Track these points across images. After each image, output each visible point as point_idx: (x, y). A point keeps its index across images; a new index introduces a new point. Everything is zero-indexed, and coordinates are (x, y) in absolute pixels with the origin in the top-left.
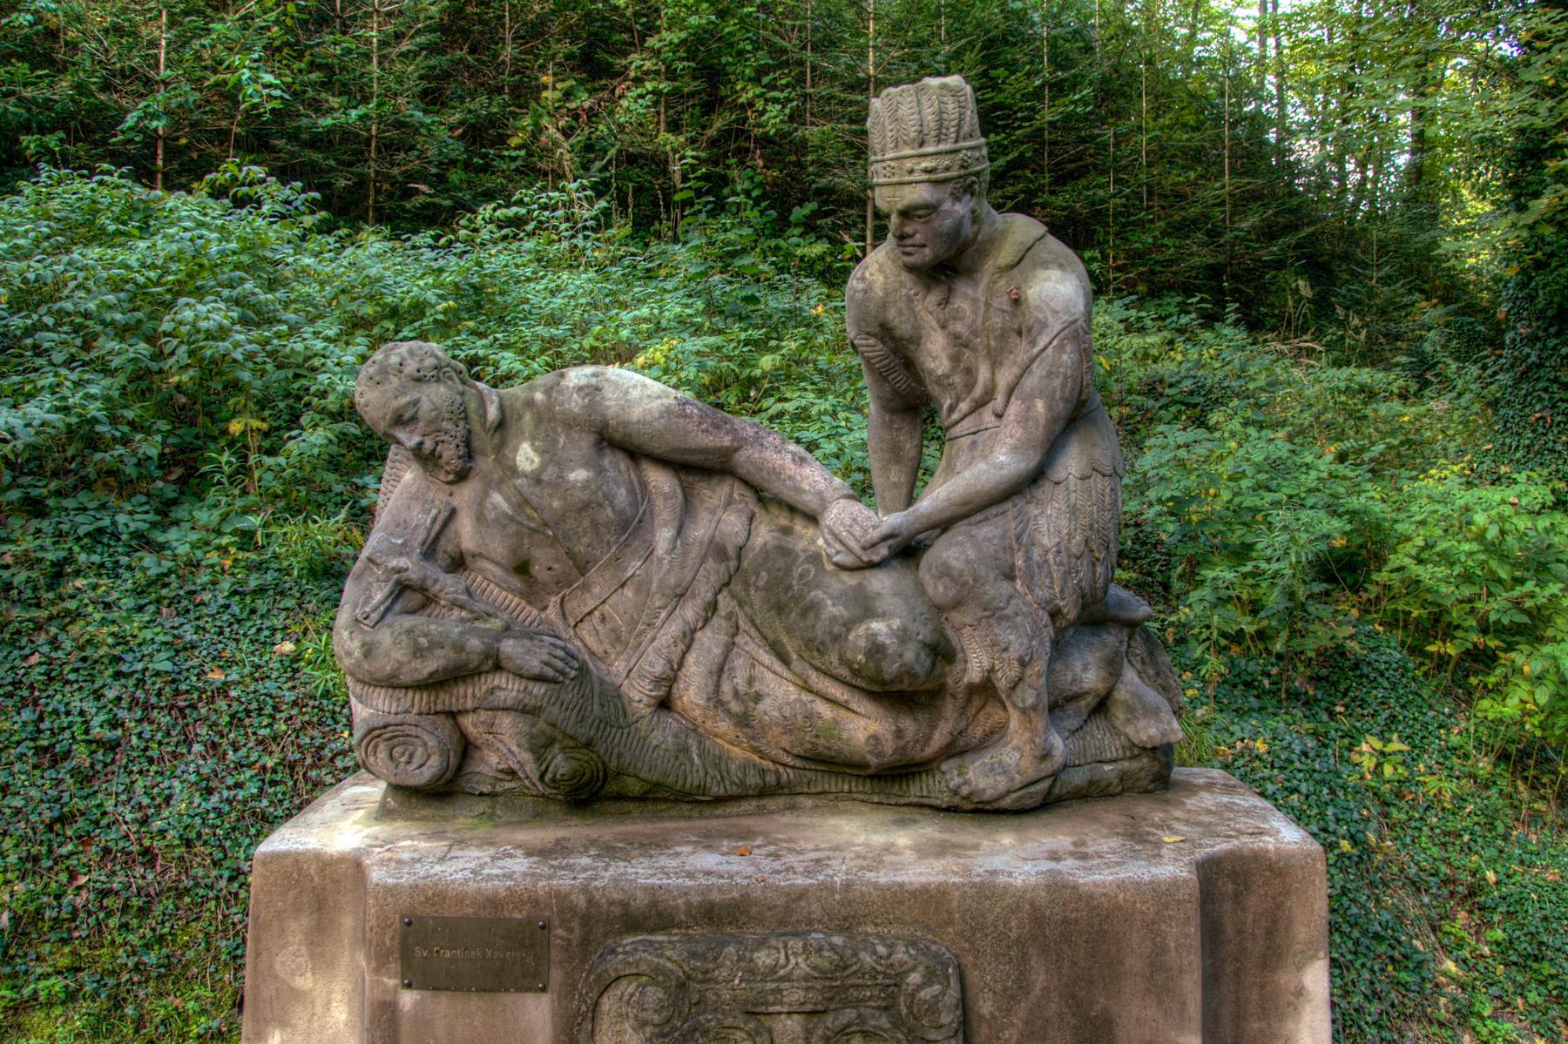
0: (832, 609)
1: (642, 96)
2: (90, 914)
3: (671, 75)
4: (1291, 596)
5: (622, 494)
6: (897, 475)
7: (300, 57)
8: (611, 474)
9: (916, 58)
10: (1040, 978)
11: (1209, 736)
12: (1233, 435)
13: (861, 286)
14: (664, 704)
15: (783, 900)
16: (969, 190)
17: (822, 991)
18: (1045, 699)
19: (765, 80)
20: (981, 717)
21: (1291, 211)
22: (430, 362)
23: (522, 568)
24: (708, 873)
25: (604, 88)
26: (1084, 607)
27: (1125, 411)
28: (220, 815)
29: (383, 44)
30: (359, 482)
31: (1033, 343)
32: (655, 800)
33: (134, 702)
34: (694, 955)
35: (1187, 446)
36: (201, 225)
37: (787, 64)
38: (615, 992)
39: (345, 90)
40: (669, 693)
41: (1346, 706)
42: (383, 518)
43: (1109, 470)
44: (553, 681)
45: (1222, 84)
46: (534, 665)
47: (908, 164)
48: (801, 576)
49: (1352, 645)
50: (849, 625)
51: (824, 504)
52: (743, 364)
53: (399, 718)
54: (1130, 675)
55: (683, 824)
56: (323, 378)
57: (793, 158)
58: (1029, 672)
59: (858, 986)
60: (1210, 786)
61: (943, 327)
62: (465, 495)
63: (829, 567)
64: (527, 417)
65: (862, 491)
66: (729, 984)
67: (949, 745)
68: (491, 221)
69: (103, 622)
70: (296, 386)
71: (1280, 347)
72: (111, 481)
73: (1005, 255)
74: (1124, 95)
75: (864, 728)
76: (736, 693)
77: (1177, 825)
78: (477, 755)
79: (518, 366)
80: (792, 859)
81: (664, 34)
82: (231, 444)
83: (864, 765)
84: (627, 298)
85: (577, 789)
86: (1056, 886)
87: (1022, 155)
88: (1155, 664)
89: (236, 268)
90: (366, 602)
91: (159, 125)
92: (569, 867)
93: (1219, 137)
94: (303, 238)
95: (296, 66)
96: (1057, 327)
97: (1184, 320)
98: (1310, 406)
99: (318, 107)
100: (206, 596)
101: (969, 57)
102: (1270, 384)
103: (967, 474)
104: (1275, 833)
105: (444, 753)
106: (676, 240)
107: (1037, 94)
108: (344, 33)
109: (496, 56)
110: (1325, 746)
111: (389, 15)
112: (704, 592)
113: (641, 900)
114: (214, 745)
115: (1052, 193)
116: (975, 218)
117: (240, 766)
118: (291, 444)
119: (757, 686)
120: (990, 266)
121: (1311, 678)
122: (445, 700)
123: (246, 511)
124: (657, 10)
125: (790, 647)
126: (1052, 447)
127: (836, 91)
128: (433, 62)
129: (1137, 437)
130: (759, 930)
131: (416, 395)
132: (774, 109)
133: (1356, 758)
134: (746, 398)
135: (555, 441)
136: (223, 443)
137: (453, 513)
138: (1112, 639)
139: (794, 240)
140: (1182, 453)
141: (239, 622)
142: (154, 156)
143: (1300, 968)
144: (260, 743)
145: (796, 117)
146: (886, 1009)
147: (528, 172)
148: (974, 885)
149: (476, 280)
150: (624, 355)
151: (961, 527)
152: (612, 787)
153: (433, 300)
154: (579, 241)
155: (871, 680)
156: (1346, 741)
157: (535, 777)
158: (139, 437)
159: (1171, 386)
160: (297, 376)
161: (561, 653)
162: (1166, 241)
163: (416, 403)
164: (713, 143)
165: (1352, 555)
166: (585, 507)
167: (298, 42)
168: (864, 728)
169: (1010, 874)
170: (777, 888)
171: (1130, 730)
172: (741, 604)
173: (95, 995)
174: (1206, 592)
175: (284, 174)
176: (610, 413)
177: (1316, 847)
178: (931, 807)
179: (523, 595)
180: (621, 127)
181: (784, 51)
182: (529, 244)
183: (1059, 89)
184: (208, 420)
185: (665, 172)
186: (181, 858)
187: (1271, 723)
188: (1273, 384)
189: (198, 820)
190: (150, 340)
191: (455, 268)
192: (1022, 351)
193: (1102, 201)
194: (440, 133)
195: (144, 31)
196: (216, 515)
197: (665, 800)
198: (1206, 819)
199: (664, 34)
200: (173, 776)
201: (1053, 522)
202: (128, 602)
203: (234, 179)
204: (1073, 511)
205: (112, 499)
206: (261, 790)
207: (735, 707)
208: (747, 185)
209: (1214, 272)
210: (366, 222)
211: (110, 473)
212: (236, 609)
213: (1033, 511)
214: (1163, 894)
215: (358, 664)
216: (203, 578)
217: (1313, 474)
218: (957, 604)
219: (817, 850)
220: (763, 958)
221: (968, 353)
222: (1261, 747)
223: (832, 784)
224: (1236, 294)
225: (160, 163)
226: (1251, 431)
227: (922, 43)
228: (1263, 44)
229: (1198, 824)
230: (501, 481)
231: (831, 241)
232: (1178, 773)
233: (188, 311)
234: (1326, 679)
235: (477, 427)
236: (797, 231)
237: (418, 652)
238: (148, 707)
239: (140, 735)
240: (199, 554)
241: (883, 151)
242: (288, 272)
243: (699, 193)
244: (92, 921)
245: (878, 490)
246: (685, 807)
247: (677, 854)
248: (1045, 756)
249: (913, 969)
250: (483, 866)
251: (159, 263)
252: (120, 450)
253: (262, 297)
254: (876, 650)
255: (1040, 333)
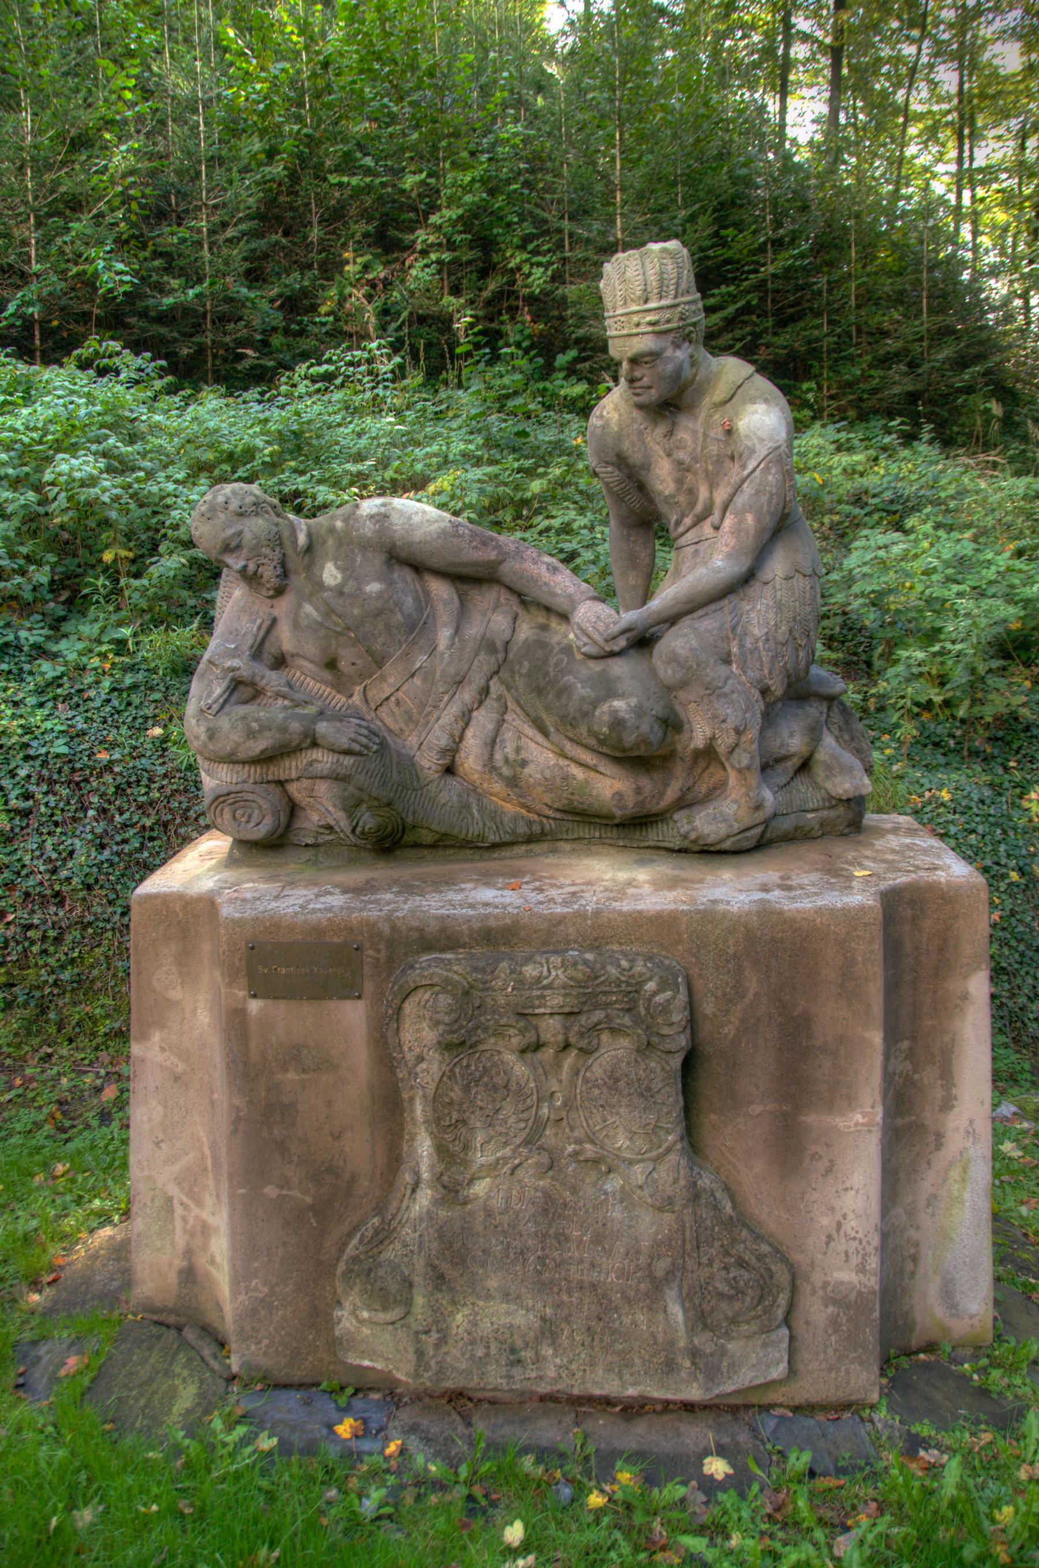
0: (582, 691)
1: (427, 266)
2: (18, 943)
3: (451, 246)
4: (973, 671)
5: (409, 602)
6: (634, 578)
7: (144, 247)
8: (400, 585)
9: (656, 222)
10: (752, 984)
11: (902, 787)
12: (926, 536)
13: (599, 423)
14: (450, 770)
15: (545, 926)
16: (687, 338)
17: (577, 997)
18: (757, 760)
19: (530, 247)
20: (705, 775)
21: (981, 343)
22: (249, 499)
23: (331, 665)
24: (486, 905)
25: (396, 260)
26: (789, 685)
27: (836, 518)
28: (112, 865)
29: (212, 232)
30: (208, 596)
31: (744, 467)
32: (445, 847)
33: (41, 779)
34: (475, 969)
35: (886, 547)
36: (72, 392)
37: (547, 232)
38: (414, 999)
39: (182, 273)
40: (453, 761)
41: (1019, 762)
42: (219, 628)
43: (809, 571)
44: (359, 754)
45: (921, 233)
46: (344, 742)
47: (635, 319)
48: (556, 664)
49: (1024, 712)
50: (595, 704)
51: (574, 605)
52: (517, 488)
53: (239, 788)
54: (829, 741)
55: (467, 866)
56: (175, 514)
57: (556, 313)
58: (743, 739)
59: (605, 993)
60: (895, 830)
61: (669, 455)
62: (283, 607)
63: (579, 657)
64: (330, 542)
65: (607, 595)
66: (503, 990)
67: (680, 799)
68: (306, 377)
69: (14, 717)
70: (154, 521)
71: (967, 461)
72: (14, 604)
73: (719, 393)
74: (836, 246)
75: (609, 787)
76: (507, 760)
77: (867, 863)
78: (302, 814)
79: (331, 497)
80: (553, 893)
81: (444, 211)
82: (106, 570)
83: (611, 817)
84: (420, 437)
85: (381, 840)
86: (765, 912)
87: (748, 302)
88: (850, 731)
89: (102, 427)
90: (209, 696)
91: (34, 311)
92: (376, 902)
93: (919, 281)
94: (155, 399)
95: (142, 255)
96: (764, 452)
97: (887, 440)
98: (993, 510)
99: (161, 289)
100: (92, 693)
101: (702, 220)
102: (959, 493)
103: (690, 577)
104: (945, 868)
105: (276, 814)
106: (460, 385)
107: (762, 249)
108: (179, 225)
109: (305, 238)
110: (1000, 795)
111: (216, 207)
112: (478, 679)
113: (433, 927)
114: (105, 811)
115: (775, 334)
116: (693, 362)
117: (125, 826)
118: (152, 569)
119: (523, 755)
120: (707, 402)
121: (990, 739)
122: (276, 772)
123: (120, 624)
124: (438, 191)
125: (549, 721)
126: (761, 553)
127: (590, 254)
128: (254, 245)
129: (846, 540)
130: (527, 949)
131: (239, 527)
132: (538, 272)
133: (1026, 804)
134: (519, 516)
135: (354, 561)
136: (99, 569)
137: (274, 621)
138: (814, 710)
139: (558, 383)
140: (882, 553)
141: (119, 712)
142: (33, 336)
143: (965, 977)
144: (140, 807)
145: (557, 278)
146: (629, 1010)
147: (337, 335)
148: (698, 912)
149: (295, 427)
150: (415, 484)
151: (686, 621)
152: (409, 838)
153: (261, 444)
154: (380, 391)
155: (614, 748)
156: (1018, 791)
157: (348, 830)
158: (32, 568)
159: (874, 496)
160: (155, 513)
161: (365, 732)
162: (872, 372)
163: (240, 533)
164: (489, 303)
165: (1026, 636)
166: (379, 613)
167: (142, 235)
168: (609, 787)
169: (728, 903)
170: (541, 916)
171: (828, 785)
172: (509, 688)
173: (26, 1005)
174: (900, 668)
175: (137, 346)
176: (397, 536)
177: (980, 880)
178: (671, 850)
179: (334, 686)
180: (412, 293)
181: (545, 221)
182: (338, 396)
183: (778, 244)
184: (87, 552)
185: (449, 329)
186: (84, 899)
187: (954, 776)
188: (961, 494)
189: (95, 870)
190: (38, 488)
191: (278, 417)
192: (735, 473)
193: (817, 340)
194: (262, 305)
195: (16, 233)
196: (96, 628)
197: (453, 847)
198: (890, 857)
199: (444, 211)
200: (74, 836)
201: (761, 615)
202: (31, 701)
203: (97, 353)
204: (779, 606)
205: (15, 619)
206: (142, 844)
207: (506, 771)
208: (518, 338)
209: (913, 397)
210: (206, 383)
211: (12, 597)
212: (115, 703)
213: (746, 606)
214: (851, 917)
215: (205, 746)
216: (89, 679)
217: (993, 568)
218: (684, 684)
219: (573, 884)
220: (530, 971)
221: (690, 477)
222: (945, 796)
223: (585, 832)
224: (929, 417)
225: (38, 342)
226: (941, 533)
227: (661, 210)
228: (959, 196)
229: (884, 861)
230: (311, 594)
231: (590, 382)
232: (870, 818)
233: (65, 465)
234: (1001, 739)
235: (290, 551)
236: (561, 375)
237: (251, 734)
238: (51, 782)
239: (47, 804)
240: (85, 659)
241: (614, 309)
242: (143, 427)
243: (477, 346)
244: (20, 948)
245: (618, 591)
246: (469, 852)
247: (462, 890)
248: (758, 807)
249: (650, 979)
250: (309, 902)
251: (40, 425)
252: (18, 579)
253: (123, 449)
254: (617, 723)
255: (749, 458)
